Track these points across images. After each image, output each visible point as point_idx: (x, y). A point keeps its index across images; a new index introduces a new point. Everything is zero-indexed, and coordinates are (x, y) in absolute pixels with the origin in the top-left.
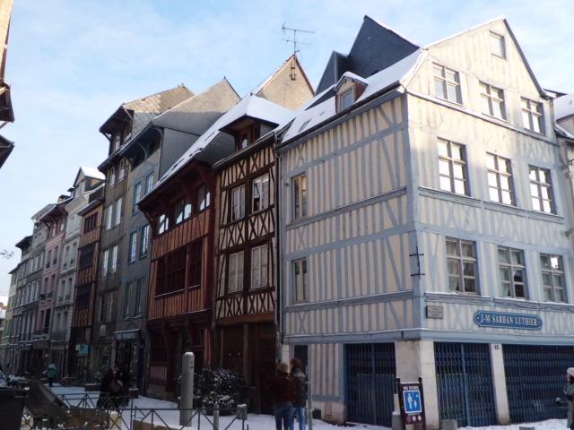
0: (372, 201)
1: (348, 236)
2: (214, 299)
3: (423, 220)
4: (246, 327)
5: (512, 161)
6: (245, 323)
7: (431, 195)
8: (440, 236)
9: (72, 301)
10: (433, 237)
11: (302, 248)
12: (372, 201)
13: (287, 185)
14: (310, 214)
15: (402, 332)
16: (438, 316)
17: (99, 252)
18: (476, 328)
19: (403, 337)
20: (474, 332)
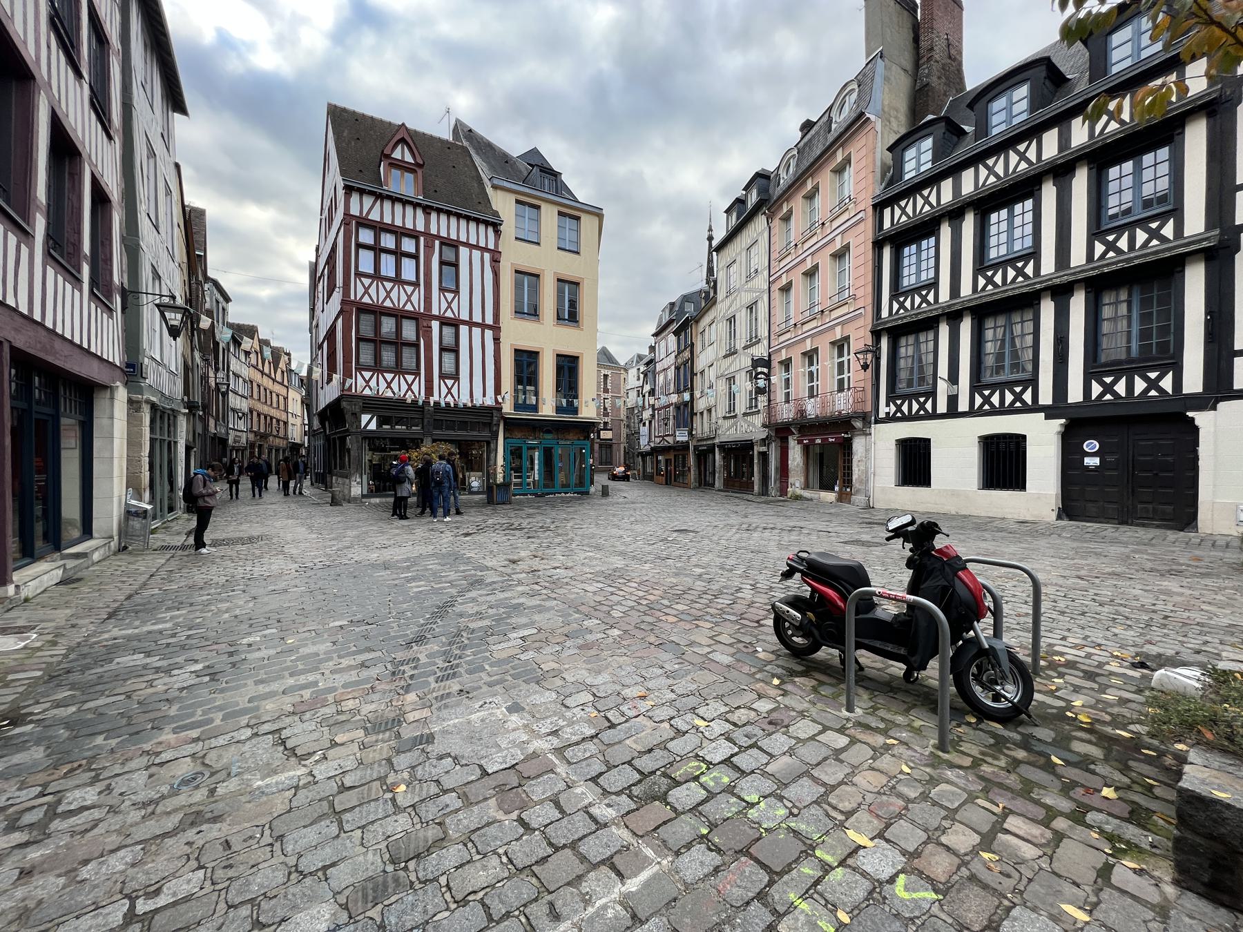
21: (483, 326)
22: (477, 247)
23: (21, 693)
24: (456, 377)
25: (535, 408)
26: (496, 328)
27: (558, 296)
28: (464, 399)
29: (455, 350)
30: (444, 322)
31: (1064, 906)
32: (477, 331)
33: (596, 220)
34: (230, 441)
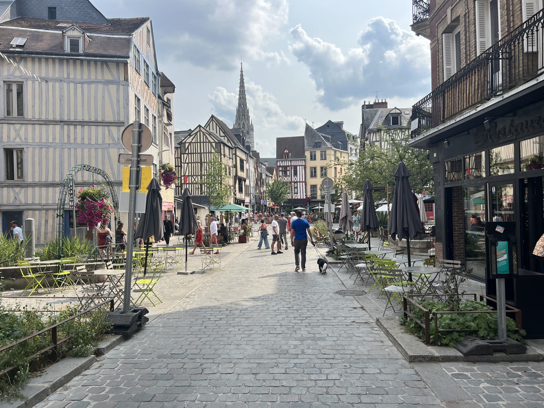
0: (97, 123)
1: (72, 141)
5: (149, 111)
11: (18, 140)
12: (97, 123)
14: (29, 113)
21: (302, 182)
22: (301, 165)
23: (220, 129)
24: (297, 193)
25: (316, 198)
26: (305, 182)
27: (22, 110)
28: (299, 198)
29: (297, 188)
30: (295, 182)
31: (356, 266)
32: (72, 85)
33: (121, 155)
34: (267, 205)
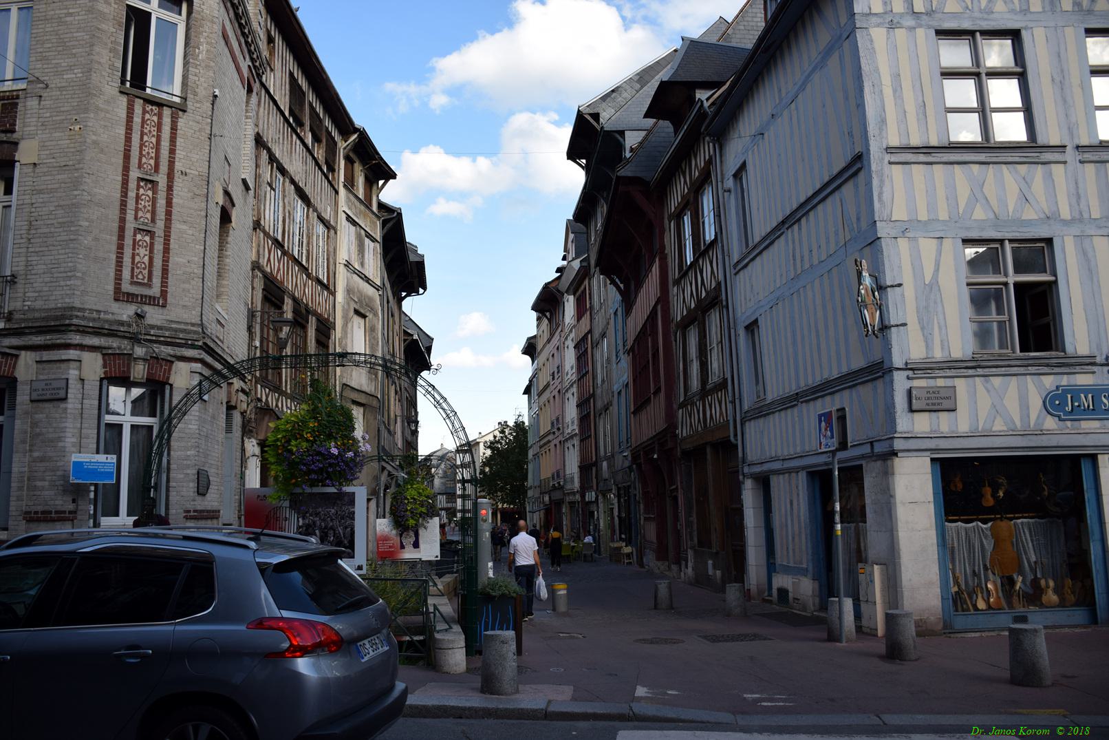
2: (675, 406)
3: (900, 213)
4: (708, 450)
6: (706, 444)
7: (922, 158)
8: (947, 243)
9: (577, 431)
10: (927, 246)
13: (729, 191)
15: (80, 453)
16: (941, 404)
17: (592, 348)
18: (1050, 423)
19: (873, 457)
20: (1050, 433)
